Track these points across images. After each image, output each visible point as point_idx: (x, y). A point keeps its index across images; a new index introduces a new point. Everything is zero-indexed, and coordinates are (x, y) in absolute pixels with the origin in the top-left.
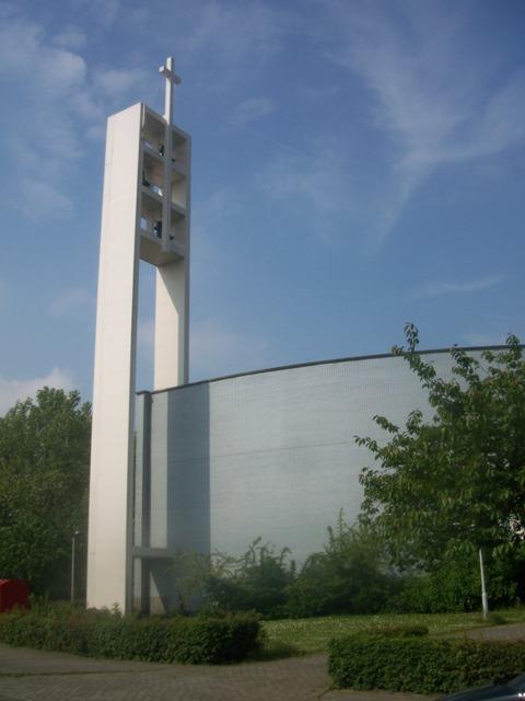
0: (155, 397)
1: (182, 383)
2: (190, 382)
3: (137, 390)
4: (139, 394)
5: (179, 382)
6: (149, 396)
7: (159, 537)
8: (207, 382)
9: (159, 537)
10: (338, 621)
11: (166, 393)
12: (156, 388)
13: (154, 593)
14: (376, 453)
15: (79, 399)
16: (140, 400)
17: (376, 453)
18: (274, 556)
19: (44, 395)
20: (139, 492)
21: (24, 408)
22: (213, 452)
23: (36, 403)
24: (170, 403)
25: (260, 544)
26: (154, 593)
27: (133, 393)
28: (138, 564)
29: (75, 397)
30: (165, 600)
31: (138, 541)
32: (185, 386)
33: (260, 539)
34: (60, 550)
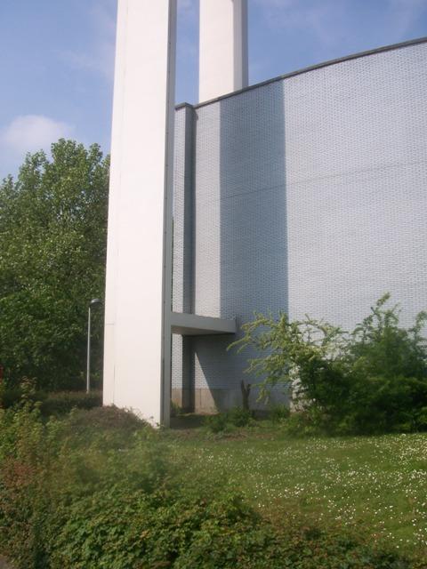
0: (200, 112)
1: (240, 88)
2: (251, 84)
3: (178, 103)
4: (178, 108)
5: (235, 87)
6: (192, 112)
7: (209, 305)
8: (279, 79)
9: (209, 305)
10: (229, 442)
11: (219, 103)
12: (202, 100)
13: (201, 382)
14: (375, 307)
15: (100, 154)
16: (181, 116)
17: (375, 307)
18: (400, 326)
19: (62, 149)
20: (179, 252)
21: (36, 163)
22: (291, 176)
23: (51, 160)
24: (223, 117)
25: (384, 308)
26: (201, 382)
27: (172, 108)
28: (178, 340)
29: (97, 153)
30: (217, 394)
31: (178, 306)
32: (244, 91)
33: (387, 297)
34: (74, 327)
